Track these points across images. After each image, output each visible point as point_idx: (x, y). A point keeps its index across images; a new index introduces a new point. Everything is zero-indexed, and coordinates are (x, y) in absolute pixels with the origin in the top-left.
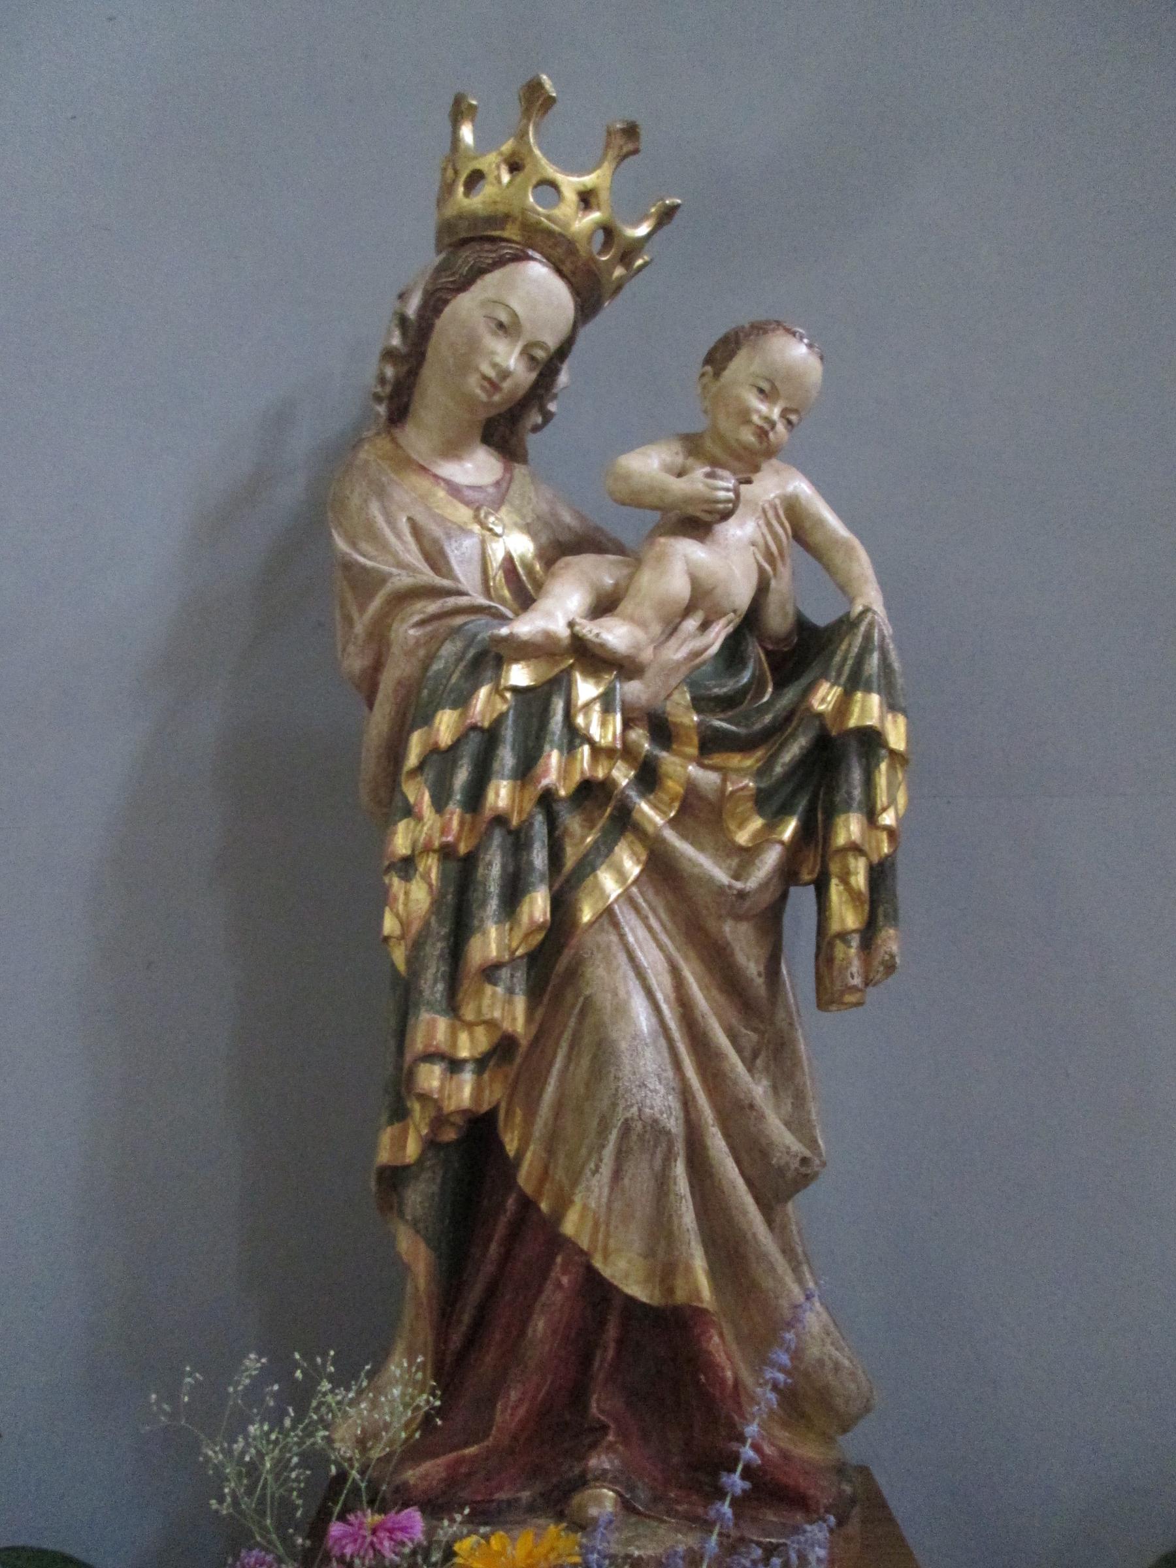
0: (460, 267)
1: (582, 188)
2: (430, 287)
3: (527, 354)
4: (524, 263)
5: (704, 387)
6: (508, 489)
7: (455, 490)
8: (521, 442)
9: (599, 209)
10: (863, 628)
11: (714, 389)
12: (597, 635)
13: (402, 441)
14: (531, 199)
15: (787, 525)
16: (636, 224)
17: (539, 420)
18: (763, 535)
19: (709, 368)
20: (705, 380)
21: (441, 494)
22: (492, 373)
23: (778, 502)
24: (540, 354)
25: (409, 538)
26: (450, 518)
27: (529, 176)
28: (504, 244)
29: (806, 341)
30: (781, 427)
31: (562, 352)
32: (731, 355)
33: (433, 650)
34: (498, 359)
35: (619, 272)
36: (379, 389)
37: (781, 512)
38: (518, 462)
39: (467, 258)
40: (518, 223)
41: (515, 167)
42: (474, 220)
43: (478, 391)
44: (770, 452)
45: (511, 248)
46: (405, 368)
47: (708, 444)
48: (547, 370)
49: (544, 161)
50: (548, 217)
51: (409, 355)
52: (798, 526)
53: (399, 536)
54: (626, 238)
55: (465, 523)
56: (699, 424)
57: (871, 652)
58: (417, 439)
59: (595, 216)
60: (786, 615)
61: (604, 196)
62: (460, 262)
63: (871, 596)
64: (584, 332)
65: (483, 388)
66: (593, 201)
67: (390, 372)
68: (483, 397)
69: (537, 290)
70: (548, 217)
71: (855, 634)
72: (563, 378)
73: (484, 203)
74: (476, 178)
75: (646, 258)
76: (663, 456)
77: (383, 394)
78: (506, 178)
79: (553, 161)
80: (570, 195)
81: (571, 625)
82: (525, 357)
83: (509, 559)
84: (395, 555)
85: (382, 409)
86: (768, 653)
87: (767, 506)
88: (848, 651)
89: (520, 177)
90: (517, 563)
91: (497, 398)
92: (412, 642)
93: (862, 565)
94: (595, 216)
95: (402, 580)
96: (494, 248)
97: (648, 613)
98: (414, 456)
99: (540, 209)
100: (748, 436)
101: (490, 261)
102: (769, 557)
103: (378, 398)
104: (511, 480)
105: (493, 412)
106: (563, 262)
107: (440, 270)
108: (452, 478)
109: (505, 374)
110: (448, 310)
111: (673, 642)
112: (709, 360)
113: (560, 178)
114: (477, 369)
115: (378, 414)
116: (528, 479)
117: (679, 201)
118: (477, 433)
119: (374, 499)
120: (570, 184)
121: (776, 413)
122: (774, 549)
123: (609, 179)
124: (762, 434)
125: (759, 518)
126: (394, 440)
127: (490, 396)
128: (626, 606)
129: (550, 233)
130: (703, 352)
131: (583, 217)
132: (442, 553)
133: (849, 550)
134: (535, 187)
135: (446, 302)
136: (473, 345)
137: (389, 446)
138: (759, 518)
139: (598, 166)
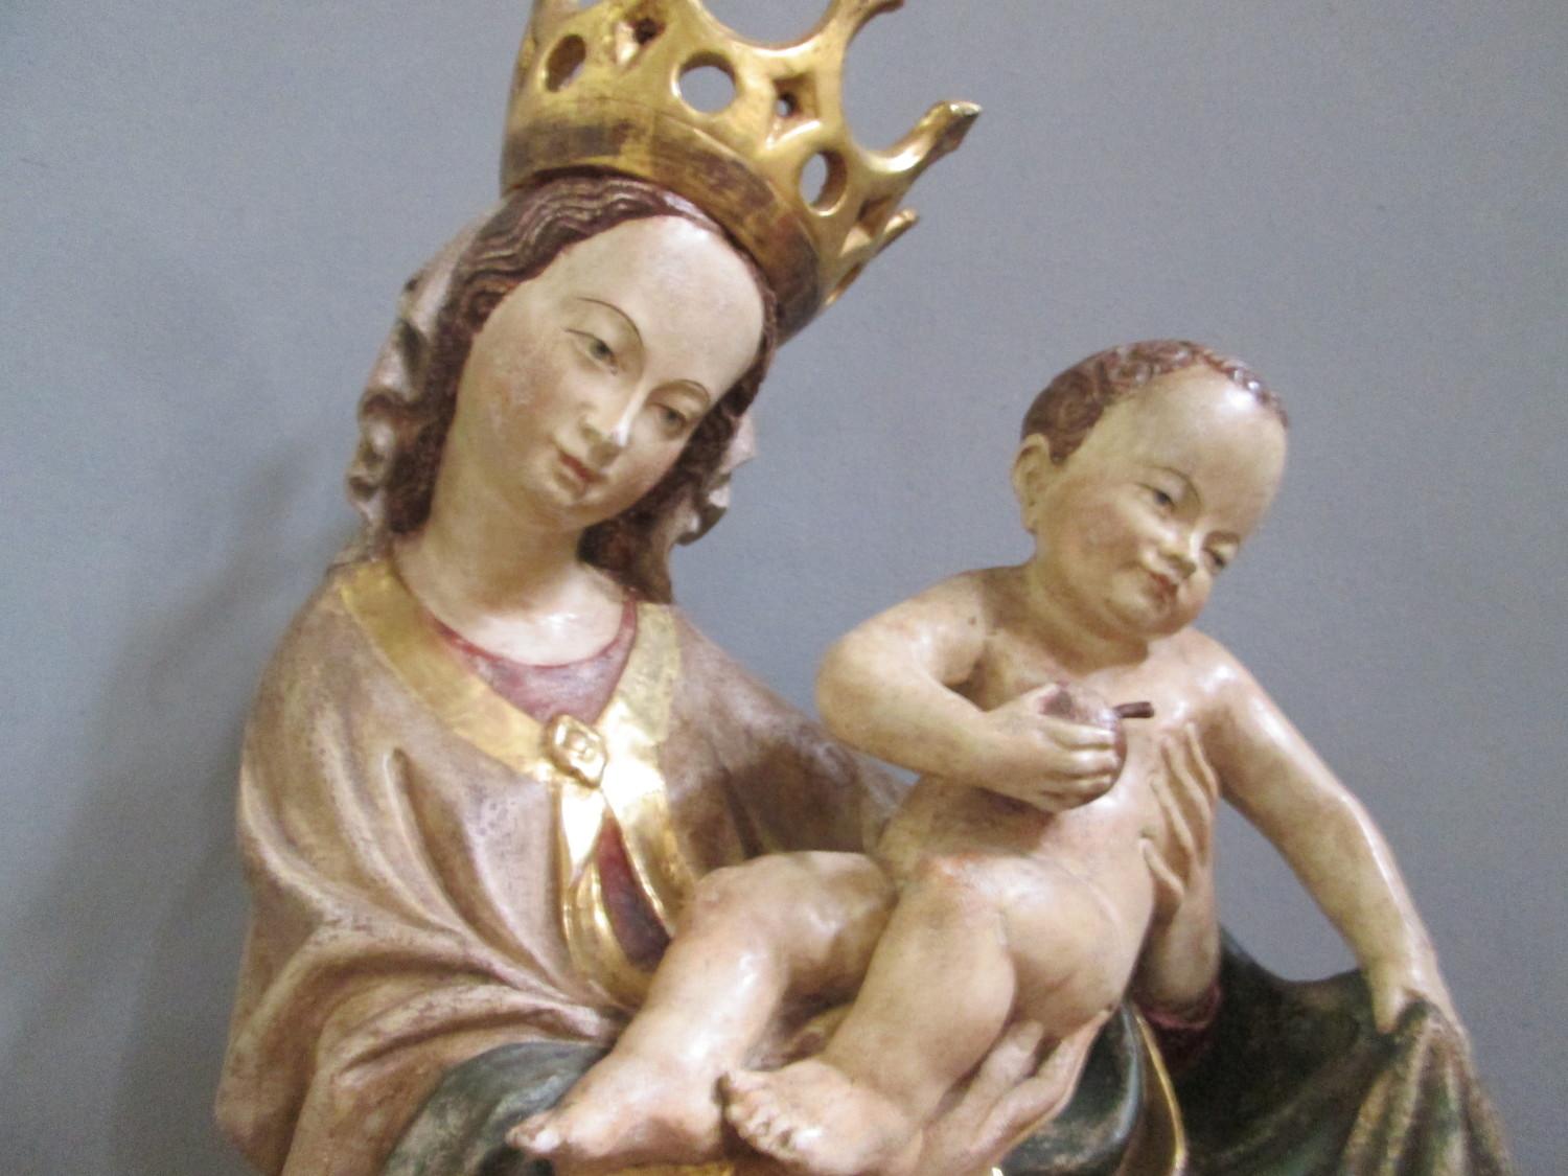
0: (524, 228)
1: (780, 71)
2: (466, 269)
3: (660, 402)
4: (656, 220)
5: (1031, 477)
6: (624, 663)
7: (508, 679)
8: (659, 565)
9: (817, 115)
10: (1417, 1062)
11: (1055, 482)
12: (785, 1138)
13: (412, 572)
14: (675, 90)
15: (1210, 776)
16: (894, 147)
17: (694, 524)
18: (1165, 811)
19: (1039, 440)
20: (1032, 462)
21: (477, 687)
22: (580, 449)
23: (1191, 728)
24: (688, 406)
25: (394, 801)
26: (490, 749)
27: (673, 43)
28: (617, 182)
29: (1252, 385)
30: (1202, 575)
31: (740, 396)
32: (1092, 416)
33: (403, 1116)
34: (594, 420)
35: (856, 239)
36: (362, 472)
37: (1198, 751)
38: (651, 599)
39: (545, 206)
40: (645, 140)
41: (646, 32)
42: (560, 134)
43: (552, 486)
44: (1171, 624)
45: (629, 190)
46: (417, 429)
47: (1038, 597)
48: (708, 437)
49: (706, 17)
50: (711, 130)
51: (414, 408)
52: (1227, 763)
53: (367, 795)
54: (869, 173)
55: (521, 759)
56: (1013, 549)
57: (1443, 1127)
58: (440, 570)
59: (808, 129)
60: (1202, 956)
61: (828, 88)
62: (525, 218)
63: (1411, 970)
64: (784, 356)
65: (562, 479)
66: (805, 98)
67: (383, 437)
68: (564, 497)
69: (684, 282)
70: (711, 130)
71: (1399, 1079)
72: (743, 443)
73: (580, 100)
74: (570, 55)
75: (908, 215)
76: (942, 629)
77: (370, 481)
78: (627, 49)
79: (722, 17)
80: (757, 83)
81: (723, 1094)
82: (656, 415)
83: (611, 834)
84: (349, 850)
85: (373, 510)
86: (1163, 1036)
87: (1171, 743)
88: (1386, 1120)
89: (656, 46)
90: (630, 845)
91: (595, 495)
92: (345, 1104)
93: (1380, 869)
94: (808, 129)
95: (341, 939)
96: (598, 190)
97: (910, 1064)
98: (433, 606)
99: (693, 113)
100: (1131, 594)
101: (585, 216)
102: (1179, 859)
103: (362, 489)
104: (633, 644)
105: (591, 520)
106: (738, 219)
107: (495, 231)
108: (506, 652)
109: (608, 452)
110: (497, 314)
111: (971, 1102)
112: (1039, 419)
113: (739, 51)
114: (550, 440)
115: (366, 522)
116: (672, 635)
117: (975, 108)
118: (571, 551)
119: (329, 706)
120: (757, 65)
121: (1193, 547)
122: (1187, 838)
123: (838, 56)
124: (1163, 589)
125: (1154, 771)
126: (396, 574)
127: (579, 494)
128: (859, 1030)
129: (712, 161)
130: (1023, 402)
131: (783, 131)
132: (459, 840)
133: (1348, 836)
134: (687, 67)
135: (494, 299)
136: (543, 392)
137: (385, 583)
138: (1154, 771)
139: (819, 27)
